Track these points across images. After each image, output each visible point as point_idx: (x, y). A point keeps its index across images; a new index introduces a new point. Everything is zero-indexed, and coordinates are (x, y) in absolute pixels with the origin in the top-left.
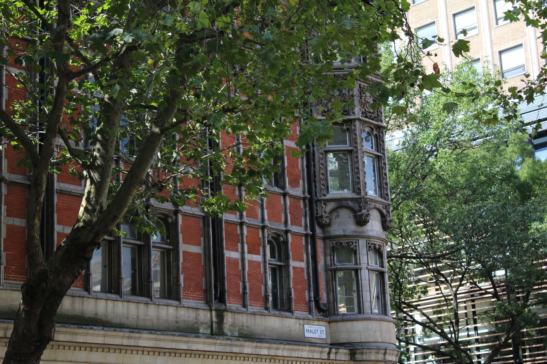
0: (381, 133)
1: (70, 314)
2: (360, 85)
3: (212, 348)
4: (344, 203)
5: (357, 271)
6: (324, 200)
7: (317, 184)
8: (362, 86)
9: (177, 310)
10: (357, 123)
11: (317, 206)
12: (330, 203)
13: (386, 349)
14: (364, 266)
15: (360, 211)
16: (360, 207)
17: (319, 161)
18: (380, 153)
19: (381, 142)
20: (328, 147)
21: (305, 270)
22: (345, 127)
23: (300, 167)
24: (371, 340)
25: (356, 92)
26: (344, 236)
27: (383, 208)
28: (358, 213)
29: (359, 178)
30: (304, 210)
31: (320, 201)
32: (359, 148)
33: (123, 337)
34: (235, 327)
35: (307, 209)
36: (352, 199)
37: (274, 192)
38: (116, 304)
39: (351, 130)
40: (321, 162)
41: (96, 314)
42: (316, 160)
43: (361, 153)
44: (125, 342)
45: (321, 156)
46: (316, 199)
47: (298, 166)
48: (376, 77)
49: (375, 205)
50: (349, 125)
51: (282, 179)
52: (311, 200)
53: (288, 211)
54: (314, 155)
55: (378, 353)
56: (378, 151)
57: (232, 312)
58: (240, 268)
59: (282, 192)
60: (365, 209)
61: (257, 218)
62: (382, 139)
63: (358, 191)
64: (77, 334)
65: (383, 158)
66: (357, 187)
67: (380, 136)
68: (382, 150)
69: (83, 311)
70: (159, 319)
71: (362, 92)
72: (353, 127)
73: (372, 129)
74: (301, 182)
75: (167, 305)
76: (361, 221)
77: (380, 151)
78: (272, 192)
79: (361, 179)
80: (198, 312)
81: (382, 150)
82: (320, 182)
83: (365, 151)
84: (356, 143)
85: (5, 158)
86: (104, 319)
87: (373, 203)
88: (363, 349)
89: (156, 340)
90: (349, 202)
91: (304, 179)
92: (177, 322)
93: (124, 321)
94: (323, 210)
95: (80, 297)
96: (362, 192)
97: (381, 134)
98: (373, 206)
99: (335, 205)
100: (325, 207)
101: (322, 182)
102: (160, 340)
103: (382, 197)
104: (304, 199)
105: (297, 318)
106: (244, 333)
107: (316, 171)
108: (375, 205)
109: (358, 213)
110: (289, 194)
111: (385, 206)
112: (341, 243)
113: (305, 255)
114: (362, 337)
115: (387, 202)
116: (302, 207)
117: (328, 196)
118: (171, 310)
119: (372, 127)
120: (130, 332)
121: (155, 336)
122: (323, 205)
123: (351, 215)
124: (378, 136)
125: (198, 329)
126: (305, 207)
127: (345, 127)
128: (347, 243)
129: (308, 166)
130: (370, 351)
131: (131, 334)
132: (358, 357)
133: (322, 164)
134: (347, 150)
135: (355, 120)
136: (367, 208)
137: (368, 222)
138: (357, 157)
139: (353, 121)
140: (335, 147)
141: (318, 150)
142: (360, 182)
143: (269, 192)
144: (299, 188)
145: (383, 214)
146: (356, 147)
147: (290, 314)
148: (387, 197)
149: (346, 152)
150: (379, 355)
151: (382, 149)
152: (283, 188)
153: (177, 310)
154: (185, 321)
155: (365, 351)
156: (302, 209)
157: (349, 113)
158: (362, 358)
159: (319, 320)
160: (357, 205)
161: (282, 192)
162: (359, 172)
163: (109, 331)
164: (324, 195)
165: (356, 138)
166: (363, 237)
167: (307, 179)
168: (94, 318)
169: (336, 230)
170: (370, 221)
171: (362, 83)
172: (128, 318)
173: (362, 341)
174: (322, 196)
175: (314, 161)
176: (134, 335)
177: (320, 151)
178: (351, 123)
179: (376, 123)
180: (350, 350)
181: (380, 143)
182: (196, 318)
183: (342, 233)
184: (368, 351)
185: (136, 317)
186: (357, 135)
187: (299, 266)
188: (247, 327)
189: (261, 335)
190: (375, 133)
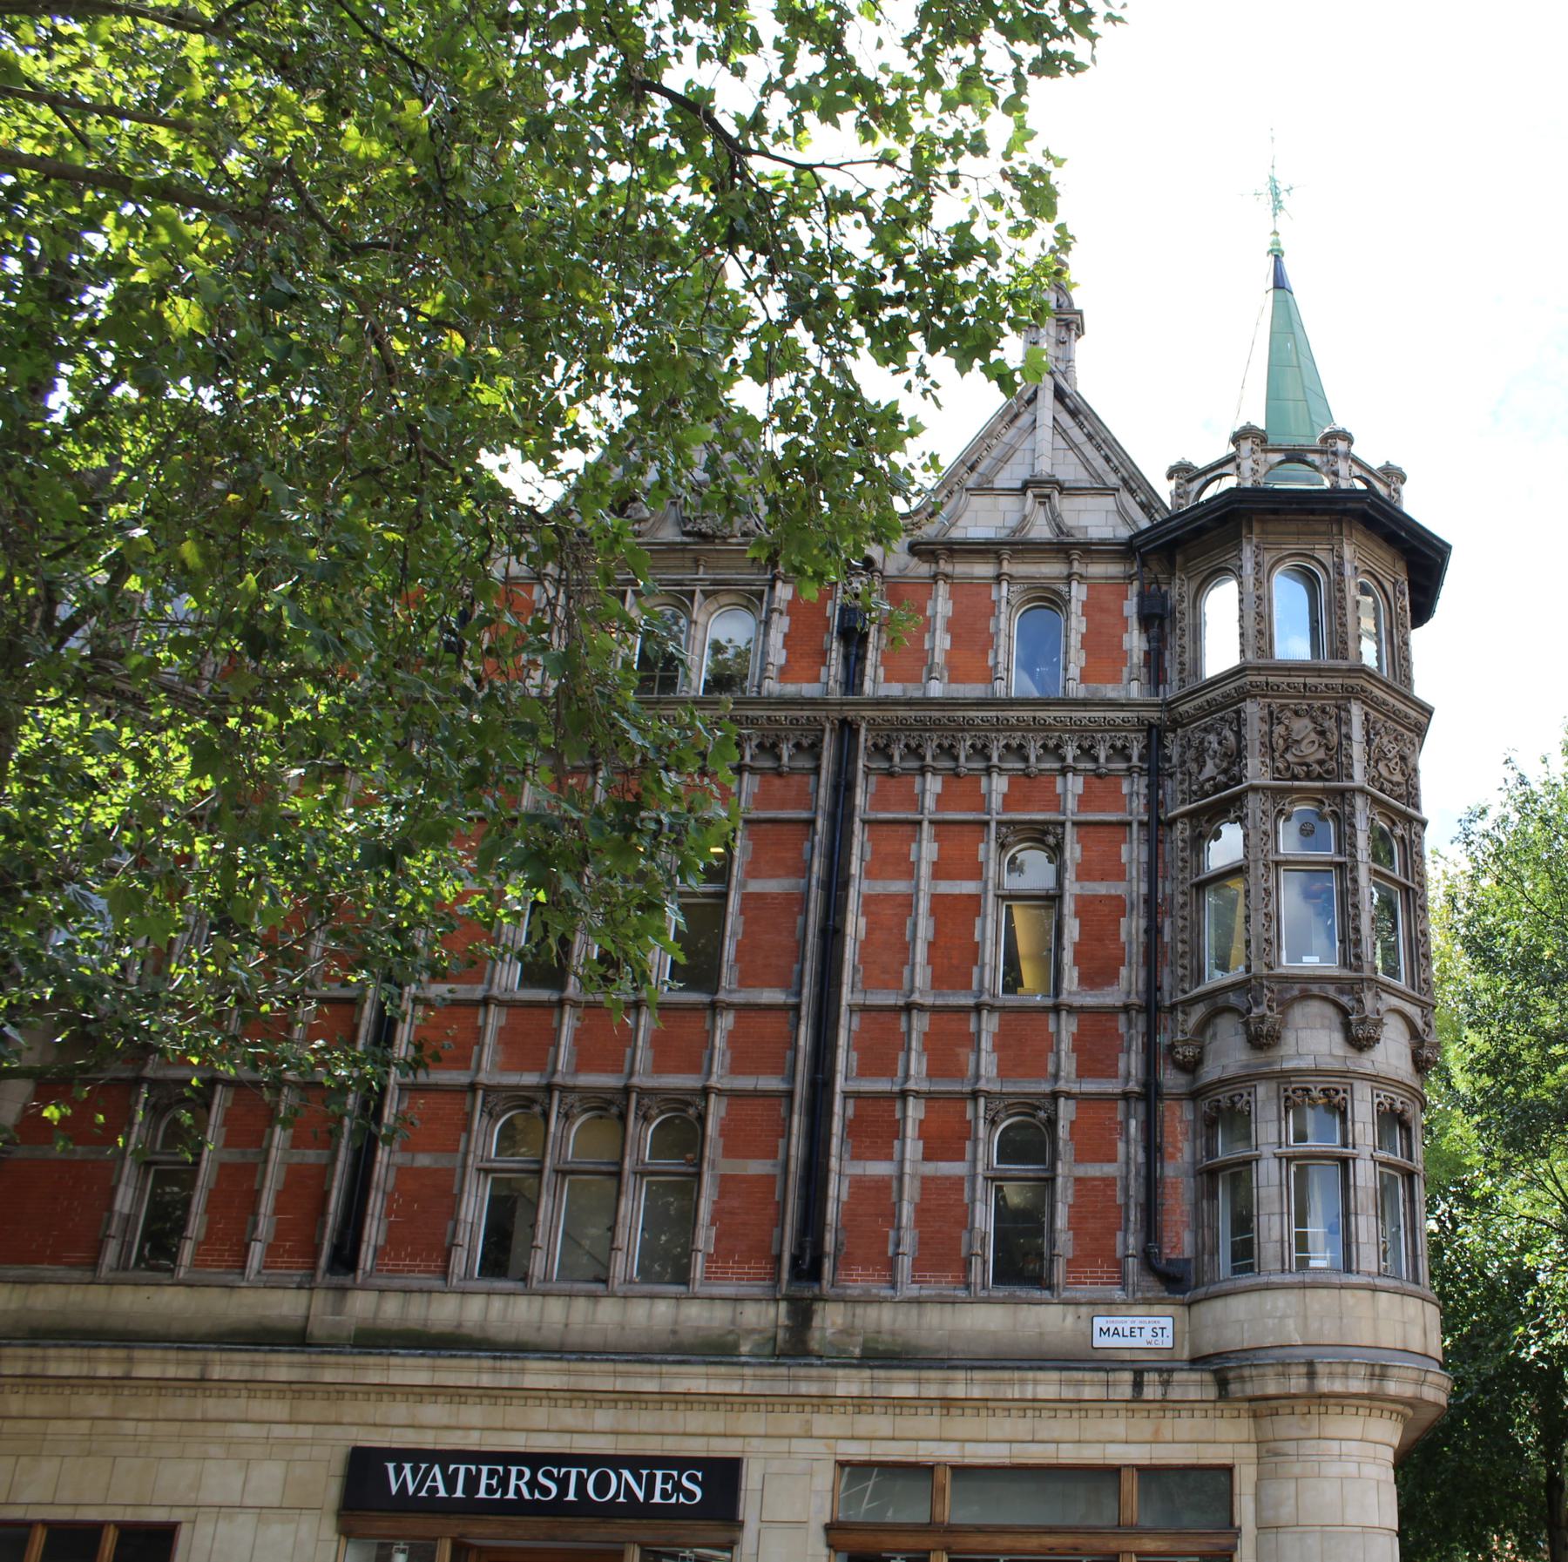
1: (395, 1327)
3: (735, 1388)
5: (1345, 1163)
6: (1183, 1002)
9: (678, 1306)
13: (1310, 1364)
24: (1268, 1342)
26: (1318, 1072)
33: (480, 1370)
34: (851, 1335)
41: (460, 1325)
44: (486, 1380)
57: (845, 1301)
64: (365, 1367)
69: (426, 1320)
70: (623, 1328)
72: (1347, 808)
75: (652, 1297)
80: (739, 1307)
86: (477, 1334)
88: (1240, 1367)
89: (568, 1373)
92: (674, 1332)
93: (529, 1336)
95: (421, 1291)
98: (1296, 993)
102: (577, 1373)
105: (1066, 1303)
106: (881, 1348)
112: (1307, 1090)
114: (1246, 1335)
118: (662, 1308)
120: (495, 1358)
121: (564, 1365)
125: (736, 1345)
128: (1323, 1090)
130: (1261, 1371)
131: (498, 1364)
132: (1234, 1388)
134: (1331, 863)
135: (1353, 791)
137: (1378, 1040)
139: (1348, 795)
146: (1353, 856)
147: (1046, 1294)
150: (1293, 1381)
153: (678, 1306)
154: (698, 1328)
155: (1246, 1372)
158: (1243, 1391)
159: (1147, 1302)
163: (439, 1356)
167: (835, 1047)
168: (452, 1334)
172: (539, 1329)
173: (1246, 1346)
176: (506, 1364)
180: (1215, 1372)
182: (733, 1322)
184: (1254, 1372)
185: (561, 1326)
187: (1098, 1174)
188: (893, 1333)
189: (938, 1351)
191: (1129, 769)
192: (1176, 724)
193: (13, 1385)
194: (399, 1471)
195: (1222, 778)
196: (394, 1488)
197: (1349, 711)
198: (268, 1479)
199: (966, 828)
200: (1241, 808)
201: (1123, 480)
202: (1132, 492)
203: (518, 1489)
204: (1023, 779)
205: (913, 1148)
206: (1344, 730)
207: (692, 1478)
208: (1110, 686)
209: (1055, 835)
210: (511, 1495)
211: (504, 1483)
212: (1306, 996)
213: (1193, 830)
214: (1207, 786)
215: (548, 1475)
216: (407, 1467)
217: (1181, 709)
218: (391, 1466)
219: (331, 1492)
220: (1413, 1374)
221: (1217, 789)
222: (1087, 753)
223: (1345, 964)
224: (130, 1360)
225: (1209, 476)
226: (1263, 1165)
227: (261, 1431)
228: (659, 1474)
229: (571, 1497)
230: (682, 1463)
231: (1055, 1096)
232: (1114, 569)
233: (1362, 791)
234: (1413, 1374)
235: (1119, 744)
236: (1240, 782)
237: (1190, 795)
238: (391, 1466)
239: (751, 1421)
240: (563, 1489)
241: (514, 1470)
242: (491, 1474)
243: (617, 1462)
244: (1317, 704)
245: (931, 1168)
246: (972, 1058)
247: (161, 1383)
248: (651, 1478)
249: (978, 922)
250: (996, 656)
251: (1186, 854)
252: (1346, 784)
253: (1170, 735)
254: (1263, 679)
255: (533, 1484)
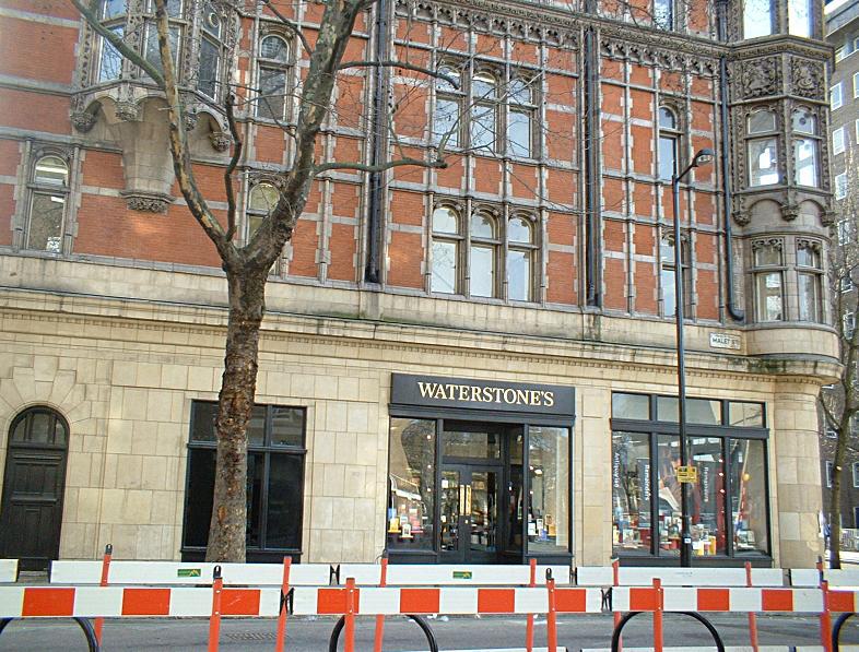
13: (816, 363)
14: (791, 267)
21: (716, 274)
25: (786, 70)
26: (767, 233)
38: (208, 340)
55: (805, 366)
58: (626, 270)
61: (621, 169)
74: (713, 175)
76: (789, 215)
84: (783, 125)
113: (716, 257)
123: (776, 207)
135: (782, 99)
146: (783, 131)
166: (791, 234)
169: (758, 225)
170: (800, 216)
177: (740, 139)
183: (764, 230)
192: (736, 57)
193: (121, 323)
194: (425, 386)
195: (765, 90)
196: (424, 394)
198: (349, 387)
203: (476, 397)
205: (329, 209)
207: (549, 395)
210: (474, 399)
211: (470, 393)
215: (488, 391)
216: (428, 385)
218: (421, 384)
219: (384, 396)
220: (833, 366)
224: (62, 303)
226: (789, 272)
227: (343, 362)
228: (533, 393)
229: (498, 401)
230: (545, 388)
231: (540, 209)
234: (833, 366)
238: (421, 384)
239: (578, 370)
240: (495, 398)
241: (473, 388)
242: (465, 390)
243: (515, 386)
245: (337, 220)
247: (166, 324)
248: (530, 394)
252: (821, 102)
254: (544, 14)
255: (482, 395)
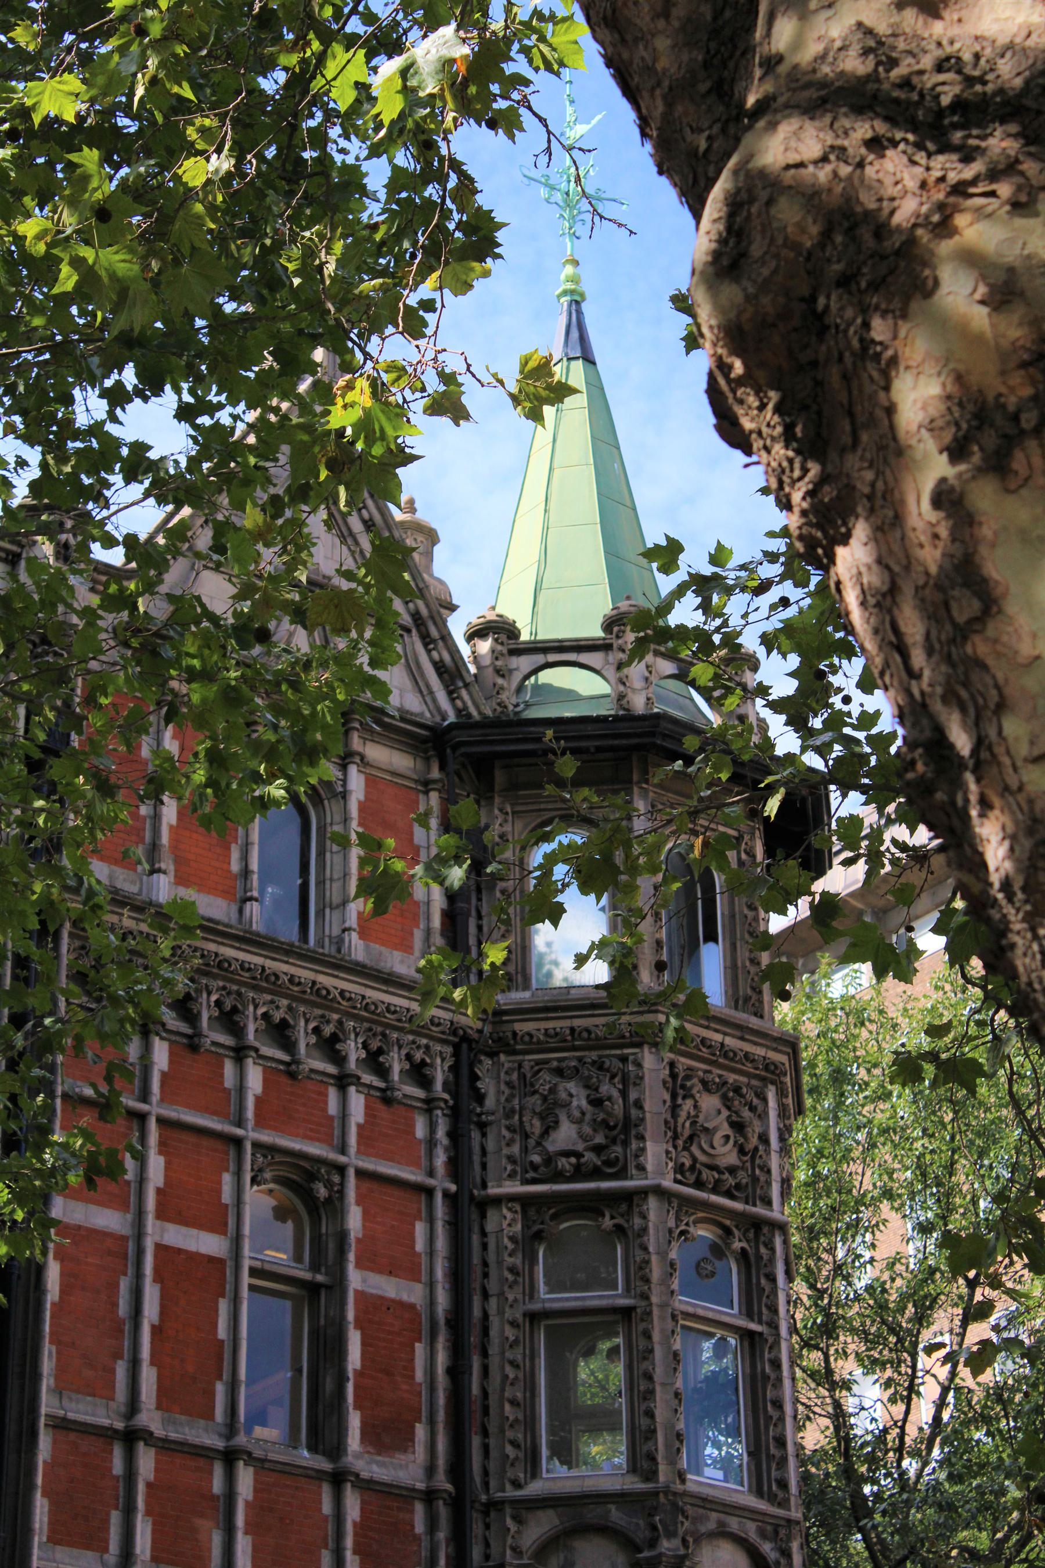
0: (766, 1245)
2: (672, 1065)
4: (592, 1514)
6: (515, 1502)
7: (492, 1442)
8: (680, 1069)
10: (653, 1204)
11: (487, 1526)
12: (540, 1513)
15: (653, 1543)
16: (654, 1528)
17: (503, 1353)
18: (760, 1322)
19: (763, 1281)
20: (544, 1301)
22: (607, 1223)
23: (419, 1375)
27: (763, 1534)
28: (645, 1554)
29: (650, 1414)
30: (425, 1543)
31: (494, 1506)
32: (654, 1299)
35: (442, 1535)
36: (621, 1498)
37: (288, 1469)
39: (630, 1233)
40: (509, 1355)
42: (493, 1350)
43: (662, 1318)
45: (510, 1333)
46: (484, 1498)
47: (413, 1370)
48: (742, 1039)
49: (721, 1524)
50: (622, 1216)
51: (335, 1419)
52: (458, 1504)
53: (349, 1542)
54: (485, 1331)
56: (750, 1315)
59: (326, 1466)
60: (671, 1535)
62: (767, 1270)
63: (646, 1465)
65: (771, 1340)
66: (645, 1448)
67: (758, 1257)
68: (764, 1310)
71: (681, 1092)
73: (728, 1231)
77: (760, 1313)
78: (279, 1467)
79: (659, 1418)
81: (764, 1310)
82: (502, 1431)
83: (682, 1313)
84: (647, 1281)
85: (148, 1513)
87: (714, 1515)
90: (613, 1508)
91: (432, 1422)
94: (509, 1541)
96: (662, 1468)
97: (763, 1250)
98: (711, 1525)
99: (557, 1522)
100: (518, 1532)
101: (509, 1434)
103: (759, 1493)
104: (429, 1496)
107: (490, 1391)
108: (721, 1524)
109: (645, 1554)
110: (357, 1475)
111: (769, 1528)
115: (781, 1512)
116: (420, 1527)
117: (534, 1488)
119: (728, 1222)
122: (509, 1522)
124: (752, 1259)
126: (432, 1525)
127: (607, 1223)
129: (457, 1372)
133: (514, 1364)
135: (643, 1193)
136: (681, 1532)
138: (647, 1335)
139: (636, 1199)
140: (567, 1299)
141: (501, 1312)
142: (654, 1431)
143: (267, 1465)
144: (411, 1457)
145: (764, 1558)
146: (645, 1297)
148: (781, 1495)
149: (610, 1318)
151: (768, 1307)
152: (336, 1450)
156: (417, 1538)
157: (624, 1168)
160: (641, 1522)
161: (326, 1466)
162: (652, 1392)
164: (517, 1485)
165: (648, 1262)
167: (447, 1423)
171: (682, 1060)
174: (508, 1486)
175: (485, 1354)
177: (508, 1314)
178: (630, 1207)
179: (738, 1206)
181: (759, 1283)
186: (651, 1249)
190: (737, 1245)
191: (428, 1101)
197: (639, 1065)
199: (206, 1142)
200: (628, 1214)
201: (416, 616)
202: (427, 640)
204: (285, 1080)
206: (633, 1095)
208: (397, 954)
209: (329, 1184)
212: (722, 1533)
213: (526, 1226)
214: (563, 1163)
217: (519, 1027)
221: (579, 1173)
222: (374, 1061)
223: (633, 1468)
225: (552, 658)
232: (401, 761)
233: (660, 1192)
235: (418, 1056)
236: (622, 1174)
237: (530, 1173)
244: (731, 1078)
246: (217, 1539)
249: (223, 1306)
250: (245, 857)
251: (517, 1260)
253: (488, 1062)
